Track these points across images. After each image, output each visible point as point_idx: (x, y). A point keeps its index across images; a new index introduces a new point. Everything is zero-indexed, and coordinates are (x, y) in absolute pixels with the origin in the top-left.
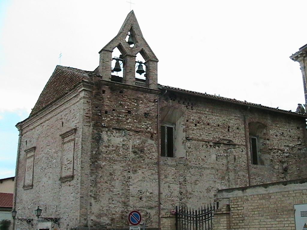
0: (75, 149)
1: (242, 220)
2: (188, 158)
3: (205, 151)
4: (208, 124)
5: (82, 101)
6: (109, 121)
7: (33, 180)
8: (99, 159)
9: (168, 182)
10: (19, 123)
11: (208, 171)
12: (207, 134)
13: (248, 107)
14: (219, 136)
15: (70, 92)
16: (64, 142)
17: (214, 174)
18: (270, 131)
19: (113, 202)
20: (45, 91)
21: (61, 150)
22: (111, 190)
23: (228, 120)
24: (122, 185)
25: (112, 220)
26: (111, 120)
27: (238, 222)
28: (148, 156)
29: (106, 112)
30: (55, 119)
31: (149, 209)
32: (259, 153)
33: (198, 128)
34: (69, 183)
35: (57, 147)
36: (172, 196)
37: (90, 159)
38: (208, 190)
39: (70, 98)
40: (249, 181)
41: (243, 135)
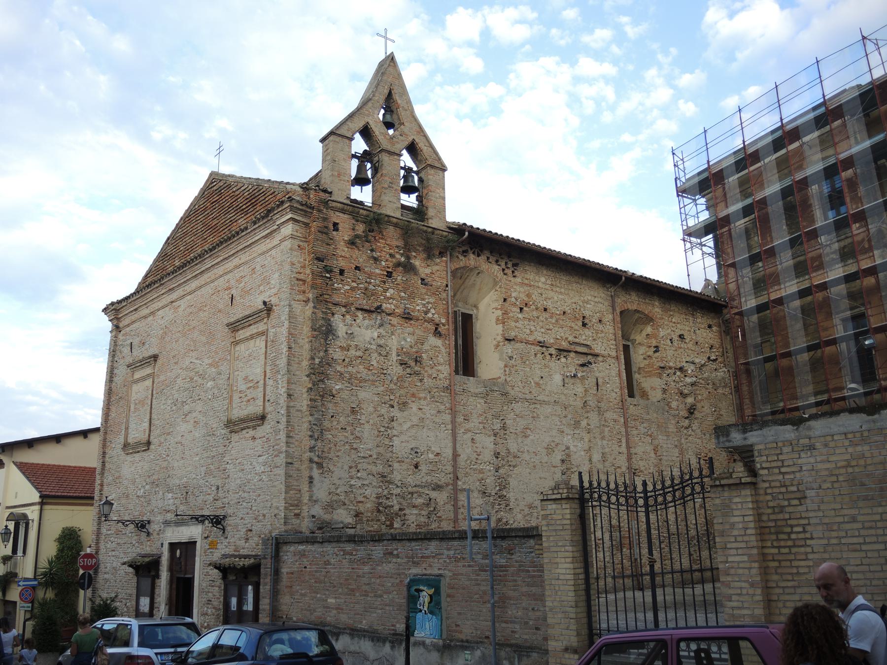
0: (268, 355)
1: (799, 499)
2: (508, 379)
3: (540, 366)
4: (545, 310)
5: (288, 244)
6: (347, 291)
7: (150, 431)
8: (327, 377)
9: (470, 431)
10: (112, 304)
11: (548, 410)
12: (543, 330)
13: (621, 277)
14: (567, 336)
15: (255, 227)
16: (237, 339)
17: (559, 415)
18: (660, 329)
19: (359, 475)
20: (180, 230)
21: (229, 358)
22: (355, 446)
23: (581, 304)
24: (378, 436)
25: (356, 516)
26: (353, 289)
27: (786, 503)
28: (430, 372)
29: (342, 272)
30: (208, 290)
31: (434, 489)
32: (636, 376)
33: (526, 316)
34: (251, 433)
35: (217, 353)
36: (480, 462)
37: (308, 376)
38: (550, 450)
39: (254, 240)
40: (627, 432)
41: (612, 337)
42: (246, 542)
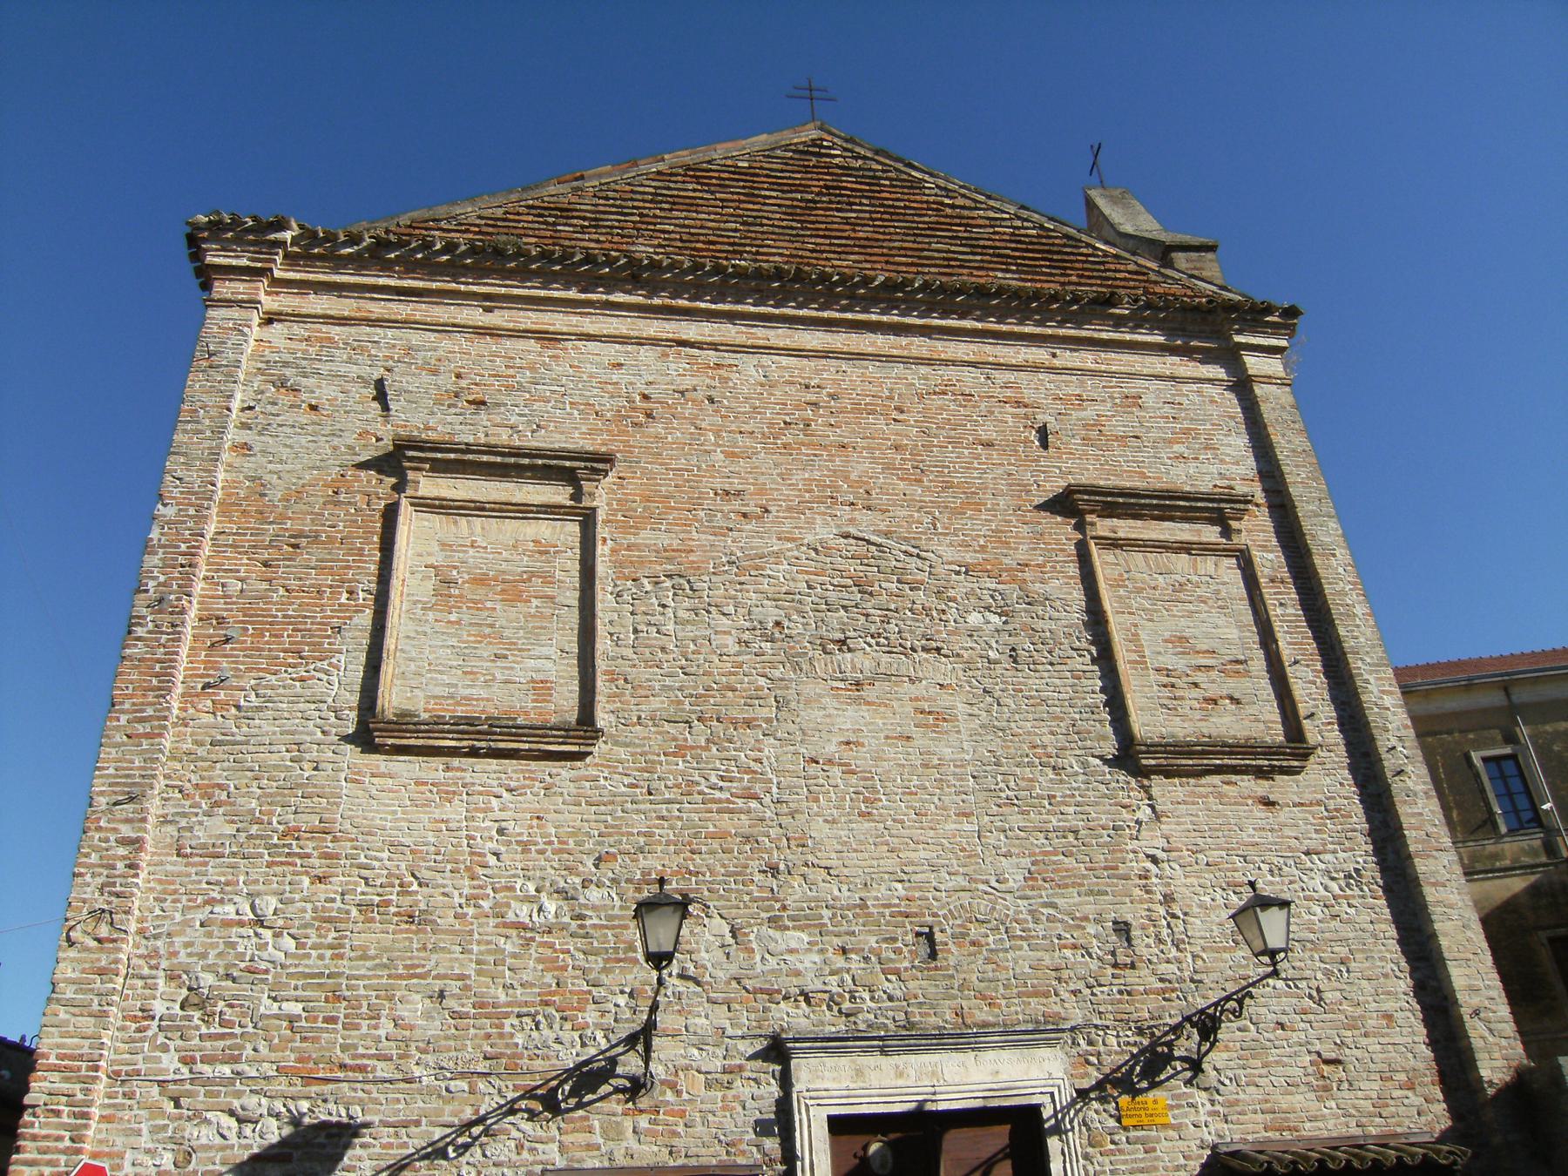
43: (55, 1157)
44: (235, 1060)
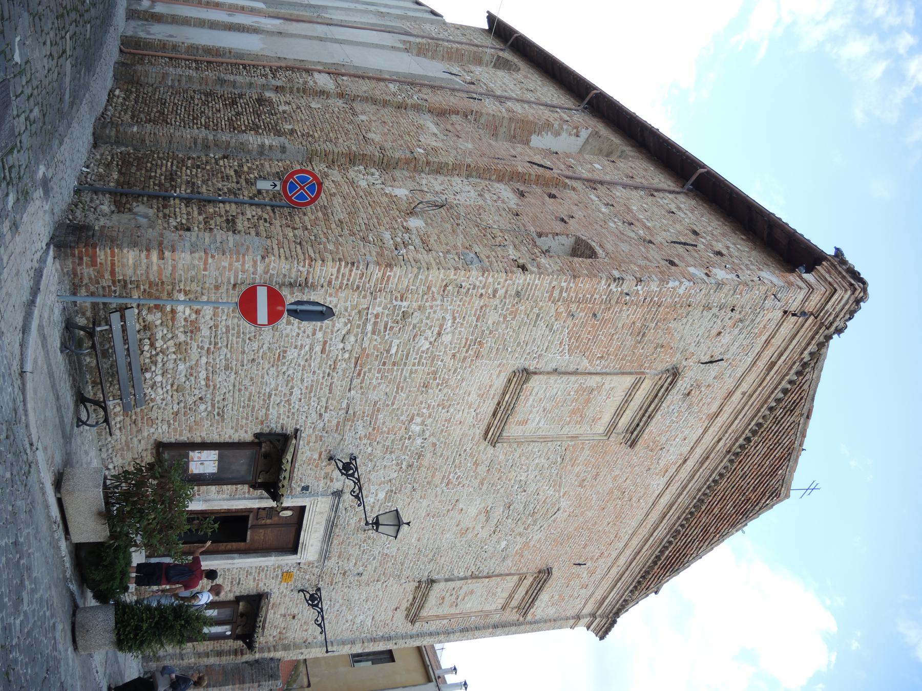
39: (615, 590)
42: (281, 615)
43: (340, 279)
44: (374, 333)
